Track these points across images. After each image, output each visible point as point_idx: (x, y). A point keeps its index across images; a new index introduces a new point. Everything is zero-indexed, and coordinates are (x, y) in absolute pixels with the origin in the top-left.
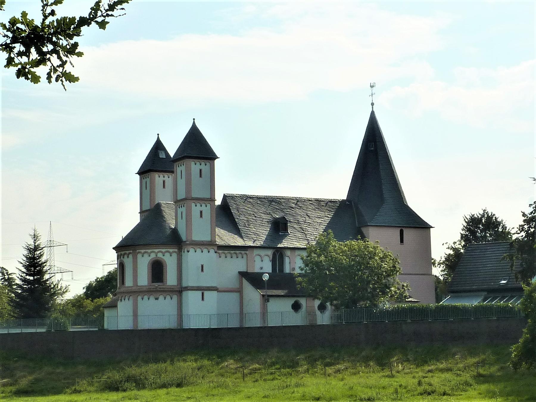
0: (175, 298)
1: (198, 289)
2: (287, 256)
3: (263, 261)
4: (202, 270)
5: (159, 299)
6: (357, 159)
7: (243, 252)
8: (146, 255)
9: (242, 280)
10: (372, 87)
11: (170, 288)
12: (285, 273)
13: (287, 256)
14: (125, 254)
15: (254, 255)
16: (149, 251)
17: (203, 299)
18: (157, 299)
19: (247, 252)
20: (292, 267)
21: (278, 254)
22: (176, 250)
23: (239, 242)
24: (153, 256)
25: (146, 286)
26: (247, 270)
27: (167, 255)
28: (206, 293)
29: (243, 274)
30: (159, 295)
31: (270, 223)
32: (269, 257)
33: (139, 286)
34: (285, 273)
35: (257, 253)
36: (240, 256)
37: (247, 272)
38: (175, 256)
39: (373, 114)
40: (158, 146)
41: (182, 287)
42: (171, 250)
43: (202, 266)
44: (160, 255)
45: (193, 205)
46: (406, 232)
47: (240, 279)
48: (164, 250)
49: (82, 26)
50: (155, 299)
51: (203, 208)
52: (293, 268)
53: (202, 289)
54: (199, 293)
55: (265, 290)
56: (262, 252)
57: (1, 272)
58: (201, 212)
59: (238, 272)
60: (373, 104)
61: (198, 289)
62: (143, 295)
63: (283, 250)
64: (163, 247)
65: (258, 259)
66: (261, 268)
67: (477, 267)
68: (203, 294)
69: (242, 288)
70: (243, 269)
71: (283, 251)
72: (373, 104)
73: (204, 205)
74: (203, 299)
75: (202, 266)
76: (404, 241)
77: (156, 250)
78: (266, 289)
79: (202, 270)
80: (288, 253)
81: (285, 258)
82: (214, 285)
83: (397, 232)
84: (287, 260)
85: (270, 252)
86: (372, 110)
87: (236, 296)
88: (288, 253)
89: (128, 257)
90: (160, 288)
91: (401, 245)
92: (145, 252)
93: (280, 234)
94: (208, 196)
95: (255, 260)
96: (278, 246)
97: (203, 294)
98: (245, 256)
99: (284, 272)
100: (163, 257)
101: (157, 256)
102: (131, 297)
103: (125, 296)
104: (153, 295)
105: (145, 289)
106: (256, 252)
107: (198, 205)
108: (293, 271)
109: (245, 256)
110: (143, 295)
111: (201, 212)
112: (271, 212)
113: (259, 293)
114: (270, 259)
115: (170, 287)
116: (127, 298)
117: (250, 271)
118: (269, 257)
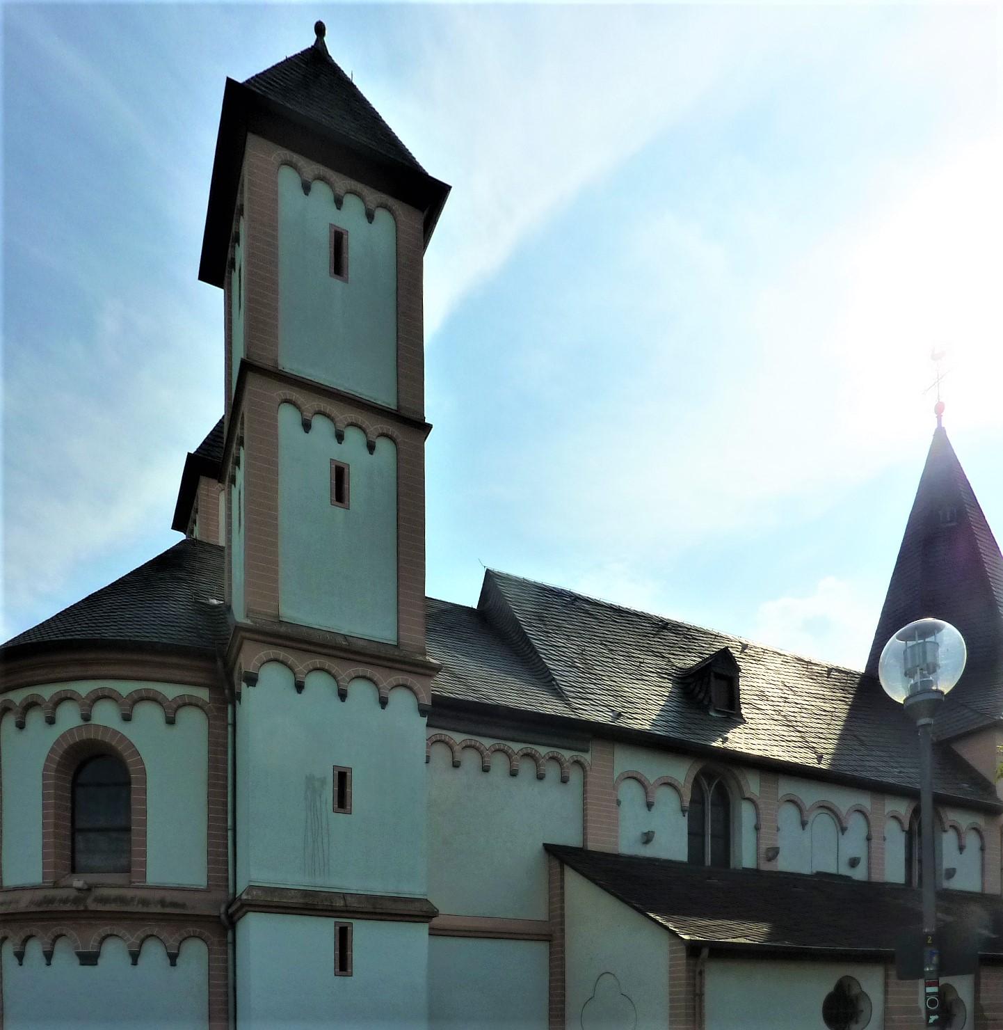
0: (195, 955)
3: (653, 809)
4: (342, 801)
5: (100, 961)
7: (567, 755)
8: (35, 719)
9: (562, 880)
12: (740, 867)
14: (31, 705)
15: (616, 775)
16: (47, 692)
18: (89, 959)
19: (586, 758)
20: (763, 847)
22: (203, 694)
23: (551, 707)
24: (69, 717)
25: (34, 888)
27: (149, 714)
28: (364, 933)
29: (558, 855)
31: (670, 680)
35: (629, 768)
36: (552, 771)
38: (194, 724)
41: (235, 899)
42: (171, 692)
43: (342, 778)
44: (106, 715)
45: (288, 418)
48: (125, 688)
50: (77, 961)
54: (323, 931)
55: (915, 640)
56: (654, 768)
58: (340, 474)
59: (541, 845)
62: (141, 934)
65: (630, 794)
66: (648, 838)
68: (343, 937)
69: (562, 923)
70: (569, 837)
72: (939, 410)
75: (342, 778)
77: (84, 688)
78: (917, 639)
79: (342, 801)
82: (412, 888)
84: (746, 815)
85: (681, 772)
86: (935, 426)
87: (540, 950)
88: (753, 784)
89: (21, 726)
90: (104, 900)
93: (713, 714)
95: (620, 798)
97: (343, 937)
98: (575, 776)
99: (732, 866)
100: (126, 730)
101: (86, 718)
102: (60, 946)
104: (121, 938)
105: (24, 903)
106: (625, 761)
109: (575, 776)
110: (141, 934)
111: (340, 474)
112: (664, 651)
113: (664, 938)
114: (682, 801)
115: (158, 895)
116: (35, 950)
117: (596, 844)
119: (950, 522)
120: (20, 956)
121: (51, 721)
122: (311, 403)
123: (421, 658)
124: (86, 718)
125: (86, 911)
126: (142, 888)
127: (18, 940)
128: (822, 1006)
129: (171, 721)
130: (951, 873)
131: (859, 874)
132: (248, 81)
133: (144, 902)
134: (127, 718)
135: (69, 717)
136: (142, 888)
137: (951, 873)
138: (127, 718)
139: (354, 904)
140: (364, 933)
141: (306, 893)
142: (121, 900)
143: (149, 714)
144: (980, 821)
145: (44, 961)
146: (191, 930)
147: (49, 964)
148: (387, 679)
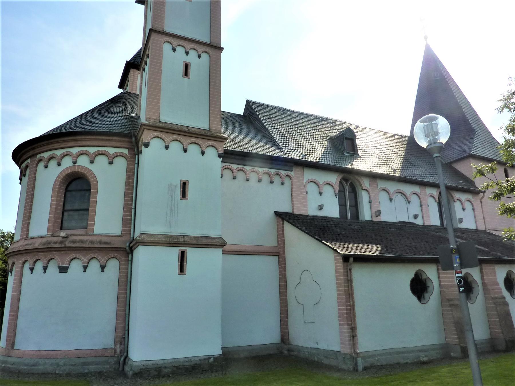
2: (364, 189)
3: (322, 195)
4: (184, 194)
7: (283, 173)
8: (53, 164)
9: (283, 227)
11: (100, 242)
12: (363, 220)
13: (364, 189)
16: (59, 153)
17: (182, 269)
19: (292, 174)
20: (374, 210)
21: (347, 186)
22: (126, 151)
24: (67, 163)
27: (102, 160)
28: (192, 253)
30: (68, 259)
32: (333, 187)
38: (121, 164)
40: (149, 58)
42: (112, 151)
43: (184, 185)
44: (83, 162)
47: (278, 225)
48: (92, 150)
49: (132, 68)
50: (58, 270)
51: (192, 58)
52: (376, 212)
54: (174, 253)
56: (322, 177)
57: (2, 259)
58: (186, 67)
63: (359, 178)
65: (312, 188)
68: (182, 255)
69: (284, 247)
70: (286, 208)
71: (358, 181)
74: (182, 269)
75: (184, 185)
77: (75, 151)
79: (184, 194)
80: (366, 183)
81: (362, 193)
82: (214, 233)
84: (364, 197)
85: (334, 179)
87: (272, 262)
88: (366, 183)
90: (74, 242)
92: (51, 158)
96: (347, 167)
97: (182, 255)
98: (287, 181)
99: (361, 218)
100: (91, 167)
101: (75, 163)
106: (309, 174)
108: (377, 216)
109: (287, 181)
111: (186, 67)
115: (99, 238)
116: (39, 266)
118: (333, 187)
120: (32, 269)
121: (59, 164)
122: (176, 42)
123: (219, 135)
124: (75, 163)
125: (65, 247)
129: (111, 163)
130: (461, 221)
131: (419, 222)
134: (92, 162)
135: (67, 163)
137: (461, 221)
138: (92, 162)
139: (188, 240)
140: (192, 253)
142: (82, 241)
143: (102, 160)
144: (470, 197)
146: (112, 255)
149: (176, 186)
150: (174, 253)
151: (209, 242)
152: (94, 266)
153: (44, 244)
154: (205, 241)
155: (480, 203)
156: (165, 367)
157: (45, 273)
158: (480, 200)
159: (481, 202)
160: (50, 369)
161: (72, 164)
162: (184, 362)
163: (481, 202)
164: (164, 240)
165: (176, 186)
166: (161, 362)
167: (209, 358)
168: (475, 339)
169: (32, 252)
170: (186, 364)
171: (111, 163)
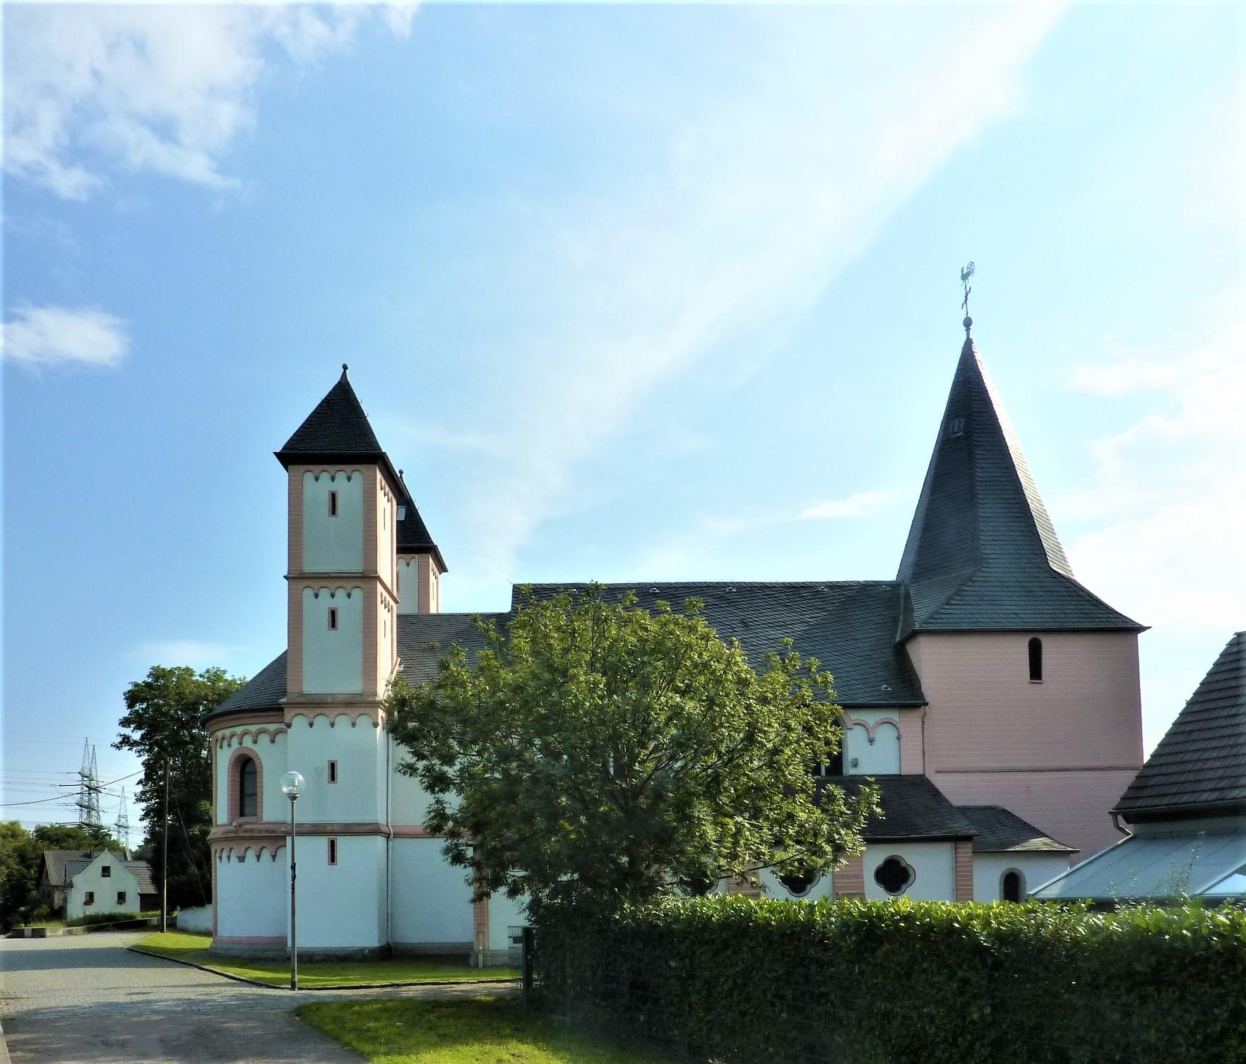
1: (315, 830)
4: (333, 777)
6: (1123, 614)
10: (965, 277)
11: (267, 831)
17: (333, 859)
26: (924, 771)
28: (341, 842)
33: (221, 826)
34: (845, 776)
37: (900, 775)
39: (968, 344)
46: (1052, 648)
48: (254, 728)
51: (340, 602)
53: (332, 833)
54: (323, 842)
58: (333, 613)
60: (968, 323)
61: (315, 830)
64: (252, 720)
67: (1231, 697)
68: (333, 844)
72: (968, 323)
73: (341, 594)
74: (333, 859)
76: (1044, 674)
79: (333, 777)
83: (1018, 649)
86: (965, 338)
90: (246, 831)
91: (1033, 685)
94: (356, 567)
97: (333, 844)
103: (231, 849)
107: (324, 594)
111: (333, 613)
115: (266, 827)
116: (225, 855)
119: (958, 432)
121: (229, 745)
122: (316, 584)
123: (372, 699)
124: (241, 743)
125: (238, 837)
126: (261, 824)
127: (228, 850)
128: (998, 881)
129: (273, 741)
132: (284, 448)
133: (260, 831)
134: (255, 742)
136: (261, 824)
138: (255, 742)
139: (336, 829)
140: (341, 842)
141: (314, 825)
142: (252, 830)
143: (264, 739)
145: (256, 859)
147: (274, 861)
148: (354, 712)
149: (323, 769)
150: (323, 842)
151: (362, 829)
152: (266, 855)
153: (227, 832)
154: (354, 829)
155: (921, 724)
156: (318, 955)
157: (229, 862)
158: (921, 720)
159: (923, 722)
160: (237, 953)
161: (239, 746)
162: (336, 951)
163: (923, 722)
164: (309, 829)
165: (323, 769)
166: (314, 950)
167: (364, 949)
168: (369, 939)
169: (217, 841)
170: (339, 953)
171: (273, 741)
